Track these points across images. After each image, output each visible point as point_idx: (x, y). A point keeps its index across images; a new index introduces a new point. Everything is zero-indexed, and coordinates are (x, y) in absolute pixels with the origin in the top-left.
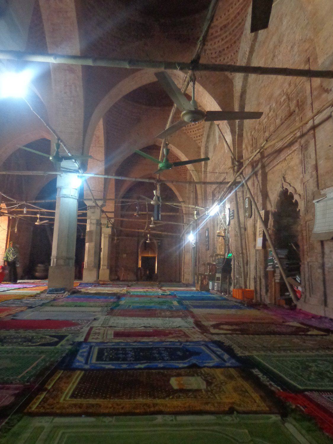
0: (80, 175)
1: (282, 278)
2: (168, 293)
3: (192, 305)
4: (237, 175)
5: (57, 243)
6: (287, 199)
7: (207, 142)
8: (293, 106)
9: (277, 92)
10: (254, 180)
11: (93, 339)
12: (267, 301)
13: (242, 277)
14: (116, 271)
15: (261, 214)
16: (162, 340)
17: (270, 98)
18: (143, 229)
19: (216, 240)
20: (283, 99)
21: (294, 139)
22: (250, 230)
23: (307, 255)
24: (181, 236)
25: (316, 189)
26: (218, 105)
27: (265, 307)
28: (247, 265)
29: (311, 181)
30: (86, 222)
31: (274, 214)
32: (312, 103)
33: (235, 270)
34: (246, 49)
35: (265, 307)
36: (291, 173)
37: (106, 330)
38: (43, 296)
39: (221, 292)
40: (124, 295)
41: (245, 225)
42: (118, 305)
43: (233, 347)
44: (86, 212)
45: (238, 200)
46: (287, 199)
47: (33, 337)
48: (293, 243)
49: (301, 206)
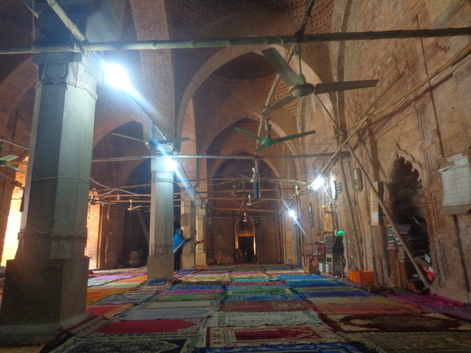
0: (175, 157)
1: (407, 258)
2: (275, 278)
3: (308, 293)
4: (342, 146)
5: (154, 231)
6: (404, 170)
7: (303, 111)
8: (402, 67)
9: (381, 54)
10: (361, 149)
11: (215, 343)
12: (391, 285)
13: (357, 257)
14: (213, 254)
15: (374, 186)
16: (291, 342)
17: (373, 61)
18: (239, 207)
19: (321, 215)
20: (389, 60)
21: (406, 103)
22: (362, 205)
23: (437, 230)
24: (280, 213)
25: (441, 156)
26: (314, 72)
27: (392, 292)
28: (362, 243)
29: (433, 147)
30: (180, 204)
31: (389, 186)
32: (425, 62)
33: (349, 249)
34: (340, 13)
35: (392, 292)
36: (407, 140)
37: (225, 331)
38: (145, 288)
39: (334, 275)
40: (229, 283)
41: (355, 199)
42: (227, 297)
43: (377, 350)
44: (180, 194)
45: (345, 172)
46: (404, 170)
47: (149, 343)
48: (414, 216)
49: (423, 176)
